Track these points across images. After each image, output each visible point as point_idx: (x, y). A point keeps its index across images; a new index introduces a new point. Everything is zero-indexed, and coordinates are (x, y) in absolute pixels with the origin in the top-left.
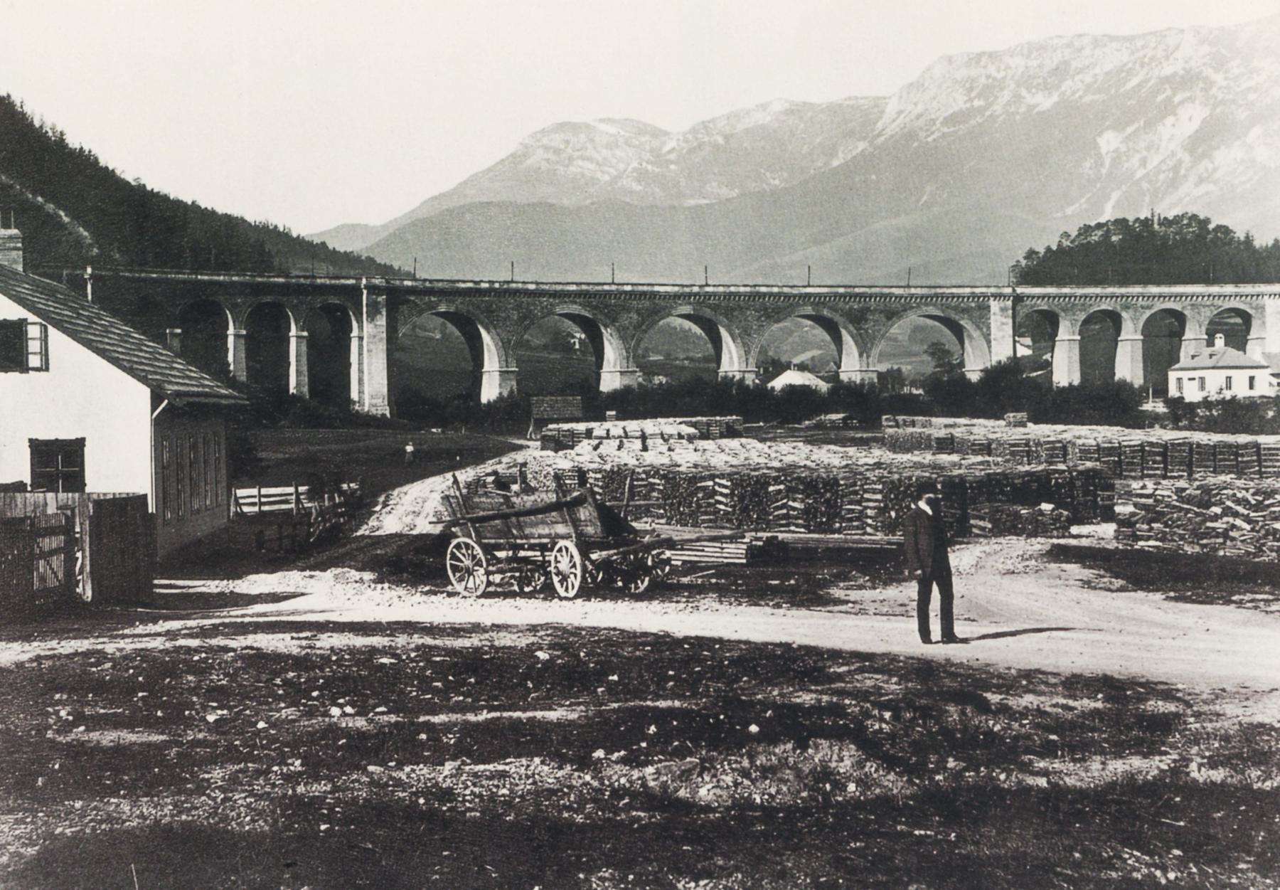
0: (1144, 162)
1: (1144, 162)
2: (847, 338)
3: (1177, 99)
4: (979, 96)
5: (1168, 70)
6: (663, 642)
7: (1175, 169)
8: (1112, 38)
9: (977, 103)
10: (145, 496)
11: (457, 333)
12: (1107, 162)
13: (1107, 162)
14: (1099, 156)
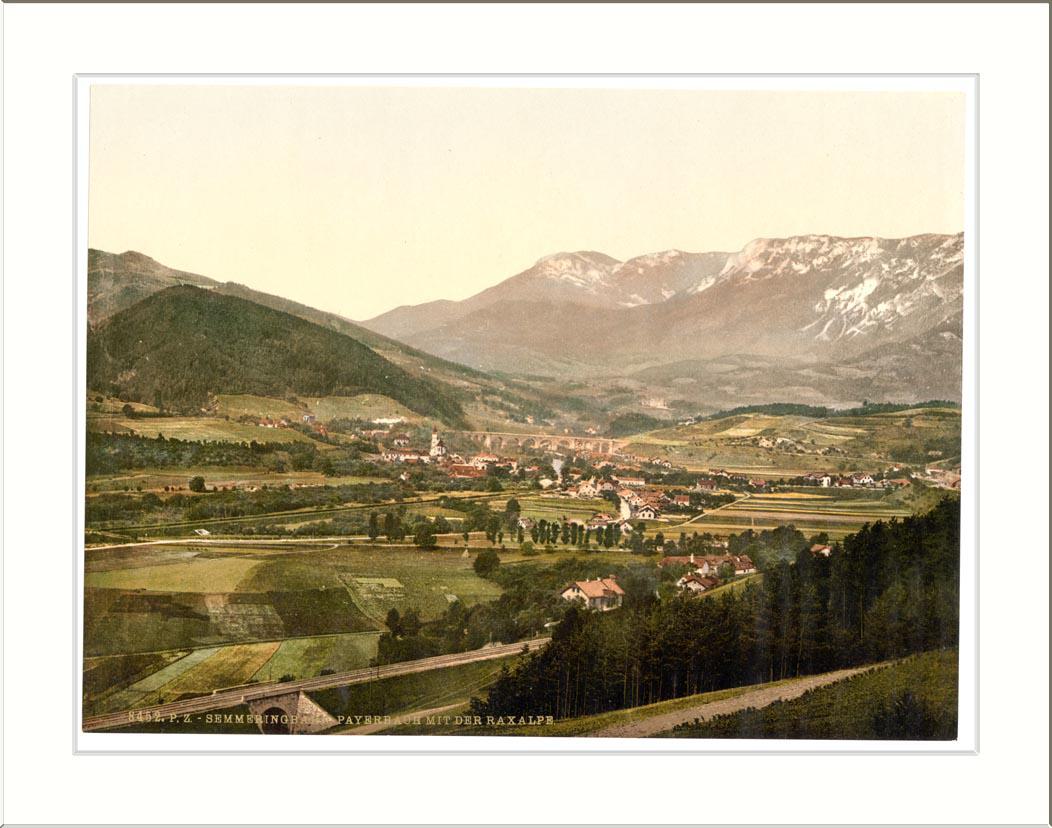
0: (846, 306)
1: (846, 306)
2: (558, 411)
3: (865, 276)
4: (771, 264)
5: (863, 260)
6: (674, 514)
7: (860, 311)
8: (840, 239)
9: (770, 267)
10: (934, 260)
11: (701, 289)
12: (828, 304)
13: (828, 304)
14: (826, 301)
